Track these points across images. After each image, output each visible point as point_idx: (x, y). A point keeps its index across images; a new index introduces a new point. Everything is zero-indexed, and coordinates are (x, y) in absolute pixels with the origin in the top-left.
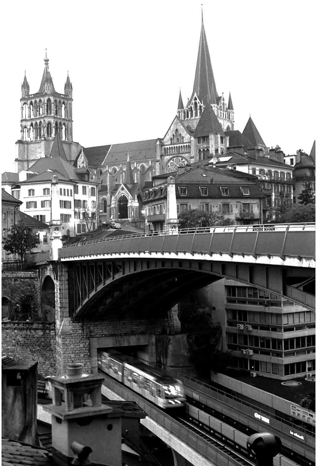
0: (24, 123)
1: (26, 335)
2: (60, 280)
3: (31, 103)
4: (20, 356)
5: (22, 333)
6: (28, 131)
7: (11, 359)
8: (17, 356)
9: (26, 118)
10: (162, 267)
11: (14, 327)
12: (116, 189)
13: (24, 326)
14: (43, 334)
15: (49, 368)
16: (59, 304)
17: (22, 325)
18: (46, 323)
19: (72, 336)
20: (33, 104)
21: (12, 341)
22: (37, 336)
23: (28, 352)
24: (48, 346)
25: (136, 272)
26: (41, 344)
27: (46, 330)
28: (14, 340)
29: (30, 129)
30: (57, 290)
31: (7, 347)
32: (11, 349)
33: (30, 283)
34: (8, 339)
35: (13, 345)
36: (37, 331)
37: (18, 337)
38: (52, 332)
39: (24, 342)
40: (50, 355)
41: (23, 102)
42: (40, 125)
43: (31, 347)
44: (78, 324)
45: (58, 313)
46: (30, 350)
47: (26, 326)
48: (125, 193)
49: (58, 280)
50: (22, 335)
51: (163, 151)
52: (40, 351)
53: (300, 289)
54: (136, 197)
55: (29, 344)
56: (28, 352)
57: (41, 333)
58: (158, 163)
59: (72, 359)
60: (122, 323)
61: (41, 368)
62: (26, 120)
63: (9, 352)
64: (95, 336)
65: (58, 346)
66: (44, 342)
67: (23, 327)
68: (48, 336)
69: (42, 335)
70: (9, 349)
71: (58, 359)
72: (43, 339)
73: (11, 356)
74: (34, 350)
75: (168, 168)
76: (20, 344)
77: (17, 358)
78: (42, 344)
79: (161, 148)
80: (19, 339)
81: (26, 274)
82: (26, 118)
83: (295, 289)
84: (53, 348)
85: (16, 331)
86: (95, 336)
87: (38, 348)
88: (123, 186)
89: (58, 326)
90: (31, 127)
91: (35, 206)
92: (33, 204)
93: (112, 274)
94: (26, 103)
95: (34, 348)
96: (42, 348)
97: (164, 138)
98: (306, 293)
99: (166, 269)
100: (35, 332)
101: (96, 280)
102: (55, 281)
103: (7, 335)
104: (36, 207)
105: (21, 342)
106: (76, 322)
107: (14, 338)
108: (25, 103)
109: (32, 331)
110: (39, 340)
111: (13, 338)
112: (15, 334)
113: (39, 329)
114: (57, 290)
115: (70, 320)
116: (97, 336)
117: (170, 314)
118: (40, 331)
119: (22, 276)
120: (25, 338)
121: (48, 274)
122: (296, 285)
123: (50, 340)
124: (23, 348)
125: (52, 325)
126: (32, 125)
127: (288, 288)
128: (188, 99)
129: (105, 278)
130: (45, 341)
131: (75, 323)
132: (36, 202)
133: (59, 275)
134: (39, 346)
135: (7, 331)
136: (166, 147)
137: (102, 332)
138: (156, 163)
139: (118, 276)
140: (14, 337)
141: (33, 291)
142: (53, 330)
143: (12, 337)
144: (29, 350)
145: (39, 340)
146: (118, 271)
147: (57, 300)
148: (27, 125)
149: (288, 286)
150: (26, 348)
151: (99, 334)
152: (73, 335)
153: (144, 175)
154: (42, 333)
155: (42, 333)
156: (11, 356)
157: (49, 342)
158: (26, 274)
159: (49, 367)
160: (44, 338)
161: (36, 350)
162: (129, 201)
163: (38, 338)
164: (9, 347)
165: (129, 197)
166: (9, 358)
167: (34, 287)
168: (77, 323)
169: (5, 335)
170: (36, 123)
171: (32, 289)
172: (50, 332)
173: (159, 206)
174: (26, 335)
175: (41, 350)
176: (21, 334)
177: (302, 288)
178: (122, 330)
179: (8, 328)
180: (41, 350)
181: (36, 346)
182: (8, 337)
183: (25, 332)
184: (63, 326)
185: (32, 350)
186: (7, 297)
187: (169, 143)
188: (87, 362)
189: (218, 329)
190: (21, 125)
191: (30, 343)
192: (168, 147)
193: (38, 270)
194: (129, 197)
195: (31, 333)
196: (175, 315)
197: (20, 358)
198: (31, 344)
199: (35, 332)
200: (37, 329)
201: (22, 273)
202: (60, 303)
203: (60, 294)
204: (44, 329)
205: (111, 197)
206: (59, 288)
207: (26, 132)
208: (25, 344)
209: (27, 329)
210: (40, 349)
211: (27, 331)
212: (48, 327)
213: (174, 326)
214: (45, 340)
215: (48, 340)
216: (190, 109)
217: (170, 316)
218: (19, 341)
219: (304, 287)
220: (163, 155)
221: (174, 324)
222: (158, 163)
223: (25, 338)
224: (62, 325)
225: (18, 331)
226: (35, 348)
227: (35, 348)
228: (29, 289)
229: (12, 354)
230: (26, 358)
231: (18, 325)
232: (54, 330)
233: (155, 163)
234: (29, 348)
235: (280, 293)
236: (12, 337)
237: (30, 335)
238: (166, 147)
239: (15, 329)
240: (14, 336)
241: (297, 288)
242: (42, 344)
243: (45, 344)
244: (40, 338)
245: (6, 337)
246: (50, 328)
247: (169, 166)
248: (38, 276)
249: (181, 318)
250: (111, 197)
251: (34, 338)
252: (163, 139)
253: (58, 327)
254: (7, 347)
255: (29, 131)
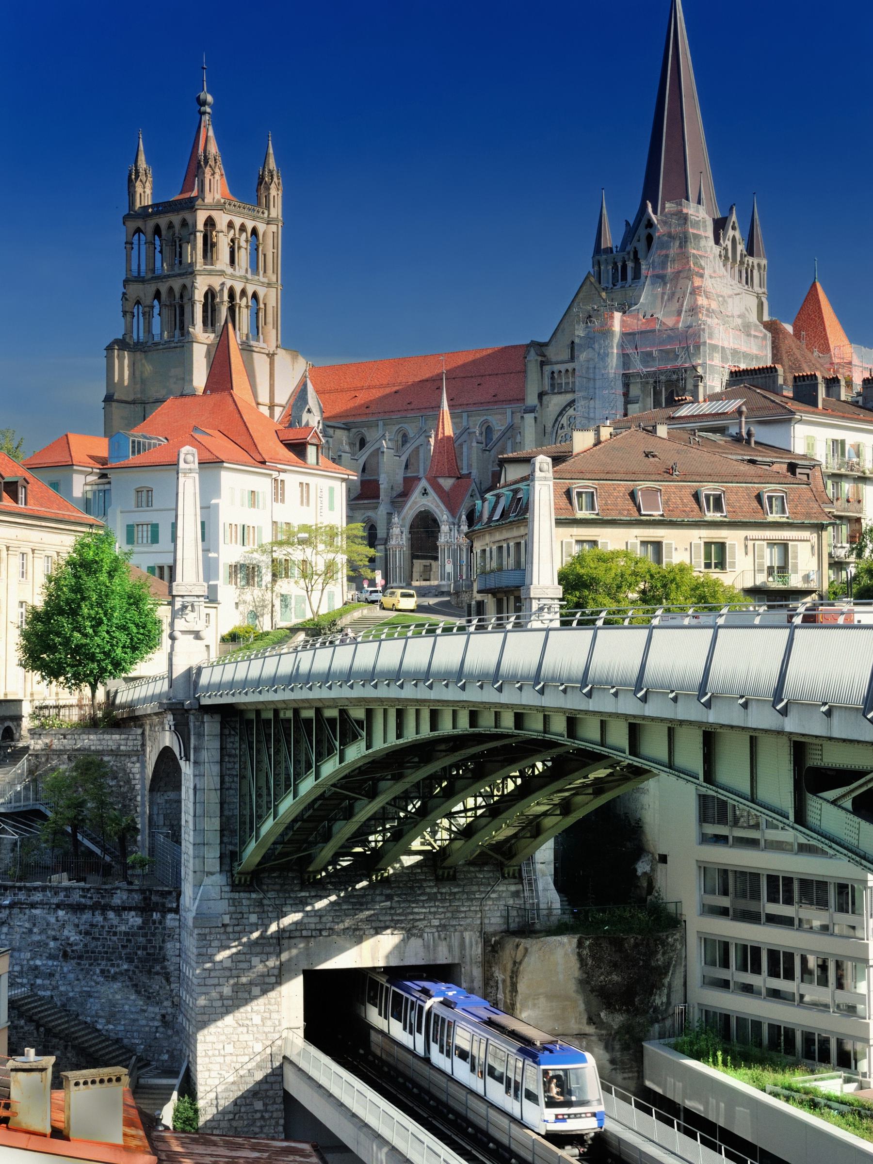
0: (135, 290)
1: (92, 925)
2: (195, 763)
3: (157, 230)
4: (69, 989)
5: (79, 918)
6: (144, 314)
7: (42, 998)
8: (62, 988)
9: (142, 274)
10: (471, 727)
11: (55, 900)
12: (405, 494)
13: (84, 897)
14: (143, 923)
15: (157, 1027)
16: (192, 833)
17: (81, 896)
18: (151, 891)
19: (229, 933)
20: (164, 232)
21: (47, 944)
22: (123, 928)
23: (95, 977)
24: (156, 961)
25: (401, 741)
26: (136, 954)
27: (153, 910)
28: (55, 939)
29: (153, 307)
30: (187, 791)
31: (32, 963)
32: (42, 968)
33: (115, 768)
34: (36, 938)
35: (51, 957)
36: (125, 915)
37: (66, 933)
38: (171, 919)
39: (86, 945)
40: (160, 987)
41: (132, 225)
42: (182, 297)
43: (104, 963)
44: (246, 895)
45: (188, 861)
46: (102, 971)
47: (91, 898)
48: (433, 503)
49: (189, 760)
50: (77, 926)
51: (547, 381)
52: (131, 973)
53: (844, 805)
54: (464, 517)
55: (100, 953)
56: (95, 977)
57: (134, 920)
58: (529, 418)
59: (225, 1002)
60: (381, 894)
61: (134, 1028)
62: (140, 279)
63: (36, 977)
64: (298, 934)
65: (188, 963)
66: (145, 948)
67: (83, 900)
68: (156, 928)
69: (140, 928)
70: (36, 967)
71: (185, 1001)
72: (141, 939)
73: (43, 988)
74: (112, 971)
75: (560, 432)
76: (73, 951)
77: (61, 994)
78: (139, 952)
79: (542, 370)
80: (68, 938)
81: (103, 742)
82: (142, 274)
83: (829, 805)
84: (172, 968)
85: (61, 913)
86: (298, 934)
87: (125, 967)
88: (424, 483)
89: (187, 899)
90: (156, 302)
91: (152, 537)
92: (146, 532)
93: (337, 744)
94: (142, 228)
95: (113, 965)
96: (137, 967)
97: (550, 340)
98: (860, 820)
99: (480, 735)
100: (120, 916)
101: (297, 762)
102: (182, 763)
103: (34, 925)
104: (155, 539)
105: (75, 948)
106: (242, 889)
107: (53, 933)
108: (138, 231)
109: (111, 915)
110: (129, 941)
111: (51, 933)
112: (58, 921)
113: (130, 909)
114: (187, 791)
115: (224, 883)
116: (304, 933)
117: (528, 872)
118: (133, 913)
119: (93, 748)
120: (87, 933)
121: (167, 743)
122: (831, 794)
123: (163, 941)
124: (79, 964)
125: (170, 898)
126: (157, 295)
127: (809, 802)
128: (627, 223)
129: (320, 757)
130: (149, 945)
131: (239, 892)
132: (155, 527)
133: (192, 746)
134: (130, 960)
135: (33, 911)
136: (556, 368)
137: (320, 922)
138: (526, 416)
139: (355, 752)
140: (54, 929)
141: (124, 793)
142: (171, 910)
143: (49, 932)
144: (98, 971)
145: (129, 941)
146: (355, 737)
147: (186, 821)
148: (142, 295)
149: (809, 796)
150: (91, 965)
151: (313, 926)
152: (230, 929)
153: (489, 451)
154: (139, 921)
155: (139, 921)
156: (43, 988)
157: (161, 948)
158: (103, 742)
159: (159, 1024)
160: (145, 935)
161: (121, 973)
162: (444, 528)
163: (126, 934)
164: (38, 963)
165: (443, 515)
166: (36, 995)
167: (128, 781)
168: (244, 891)
169: (27, 925)
170: (171, 289)
171: (120, 787)
172: (164, 917)
173: (512, 544)
174: (92, 925)
175: (134, 972)
176: (76, 921)
177: (848, 803)
178: (381, 918)
179: (37, 903)
180: (134, 972)
181: (121, 958)
182: (35, 930)
183: (87, 916)
184: (200, 900)
185: (109, 971)
186: (42, 808)
187: (566, 355)
188: (270, 1012)
189: (675, 922)
190: (124, 294)
191: (100, 949)
192: (562, 367)
193: (139, 731)
194: (443, 515)
195: (105, 919)
196: (544, 875)
197: (71, 994)
198: (106, 953)
199: (120, 916)
200: (125, 909)
201: (92, 737)
202: (195, 830)
203: (195, 803)
204: (145, 908)
205: (390, 514)
206: (192, 786)
207: (141, 315)
208: (87, 952)
209: (93, 908)
210: (132, 968)
211: (93, 915)
212: (157, 903)
213: (538, 909)
214: (150, 941)
215: (157, 943)
216: (632, 257)
217: (530, 880)
218: (71, 945)
219: (854, 799)
220: (546, 393)
221: (538, 904)
222: (533, 415)
223: (87, 933)
224: (198, 898)
225: (67, 913)
226: (118, 966)
227: (118, 966)
228: (111, 787)
229: (47, 982)
230: (90, 996)
231: (66, 896)
232: (176, 911)
233: (522, 417)
234: (99, 964)
235: (788, 819)
236: (49, 932)
237: (103, 927)
238: (556, 368)
239: (58, 906)
240: (55, 927)
241: (834, 802)
242: (139, 952)
243: (148, 954)
244: (134, 935)
245: (30, 931)
246: (163, 905)
247: (562, 427)
248: (139, 748)
249: (561, 882)
250: (390, 514)
251: (115, 934)
252: (546, 345)
253: (187, 904)
254: (32, 963)
255: (148, 315)
